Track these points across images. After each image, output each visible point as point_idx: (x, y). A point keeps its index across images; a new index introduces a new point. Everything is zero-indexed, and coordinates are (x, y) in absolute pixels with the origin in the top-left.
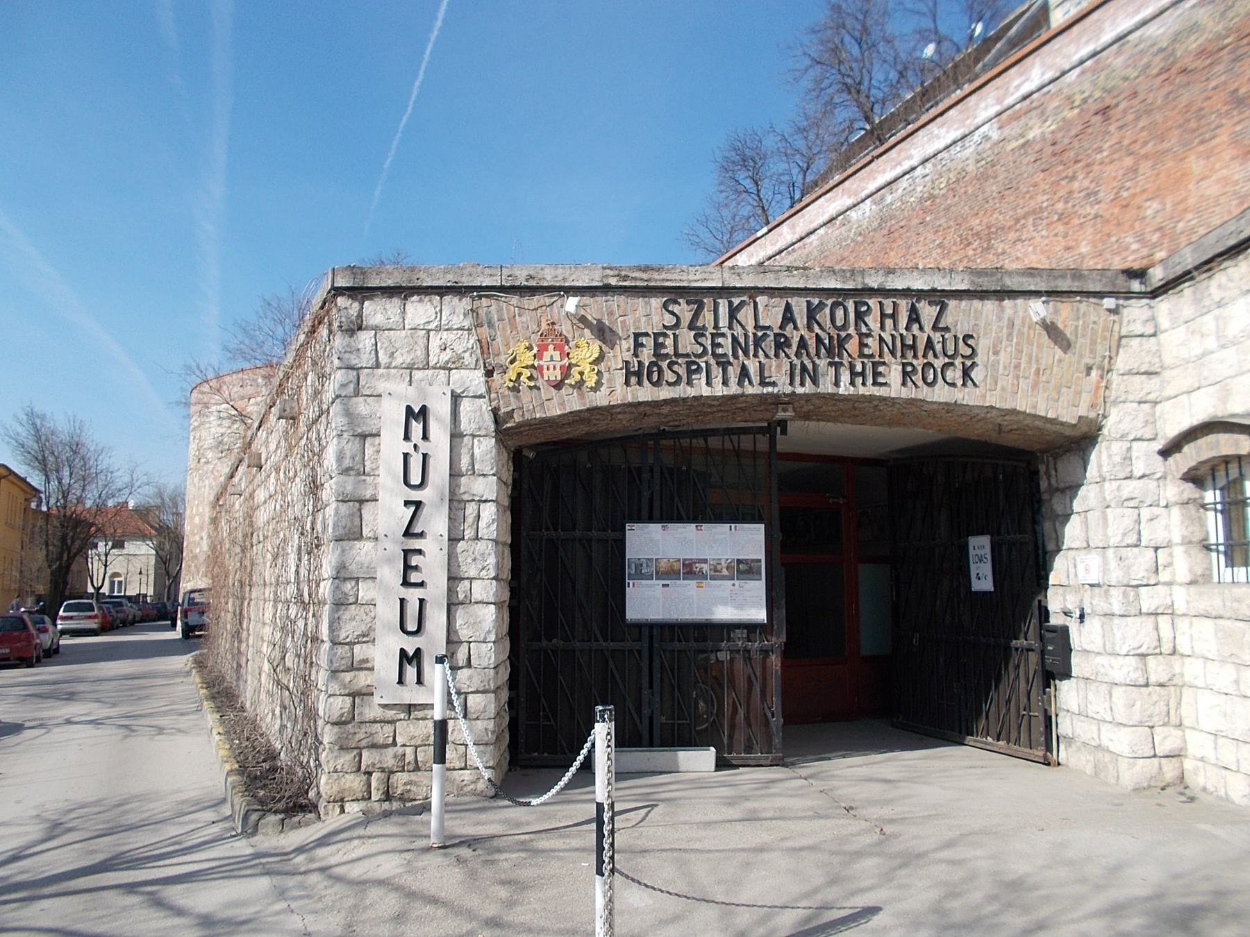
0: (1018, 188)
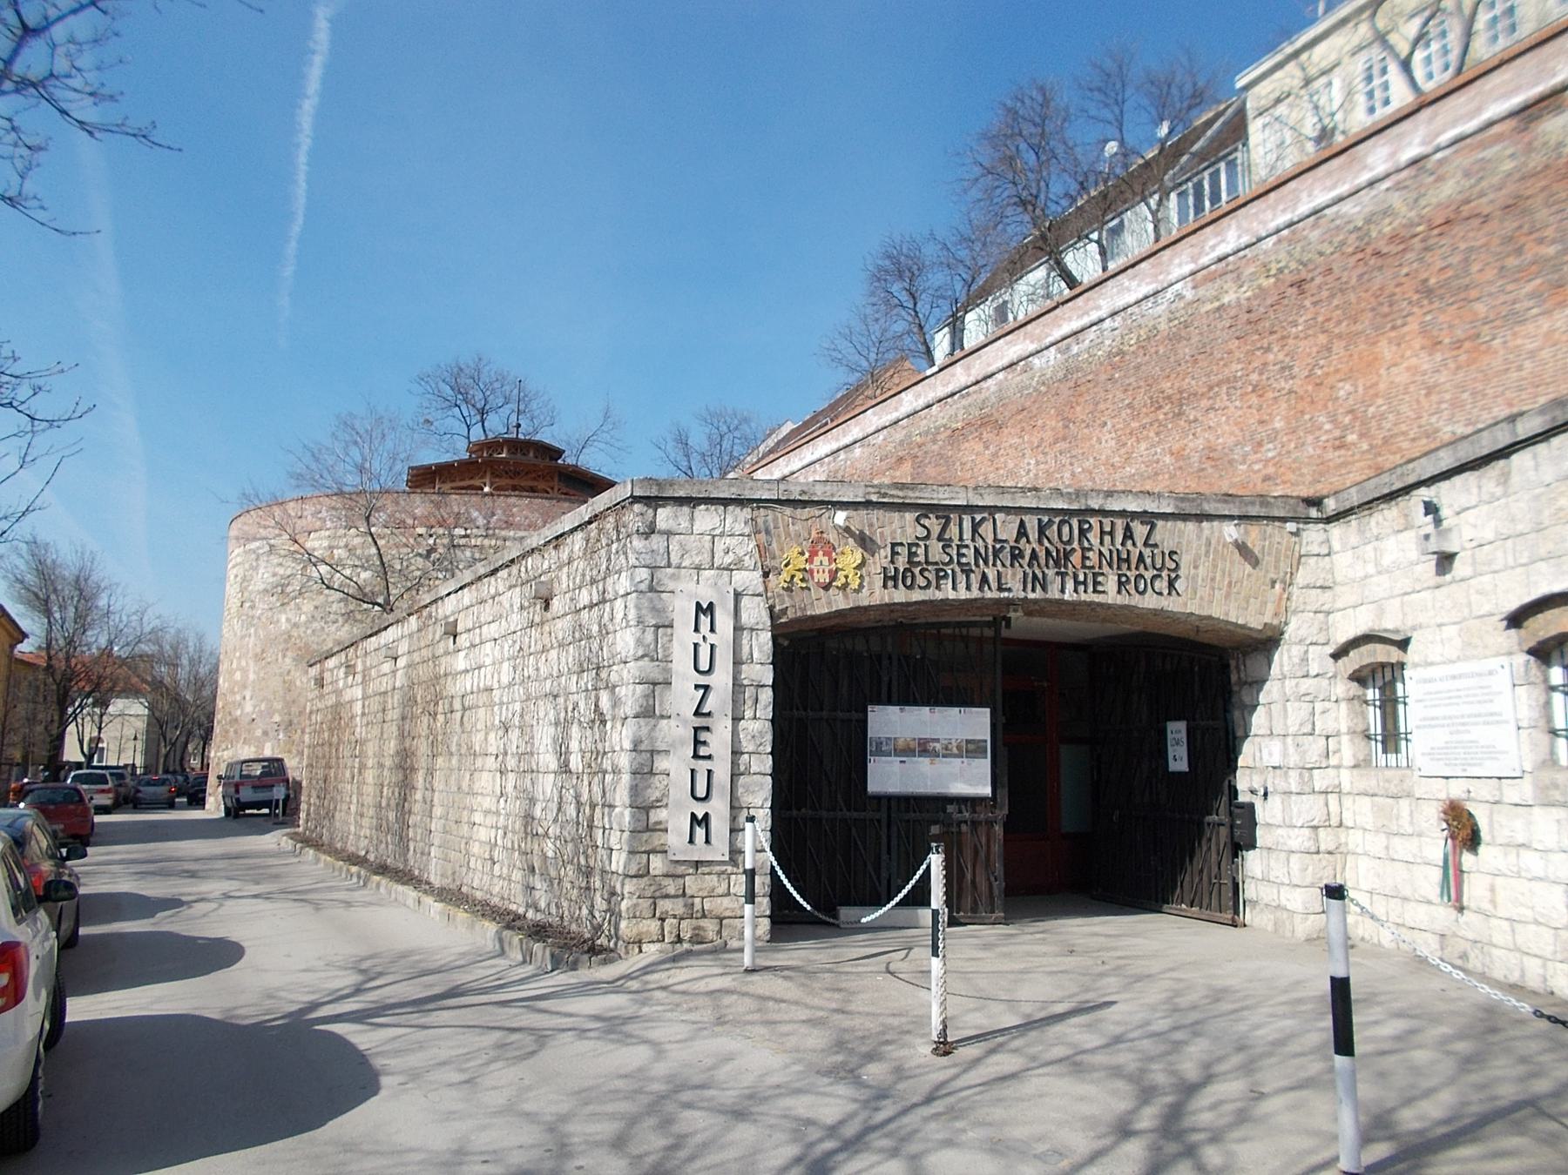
0: (1212, 354)
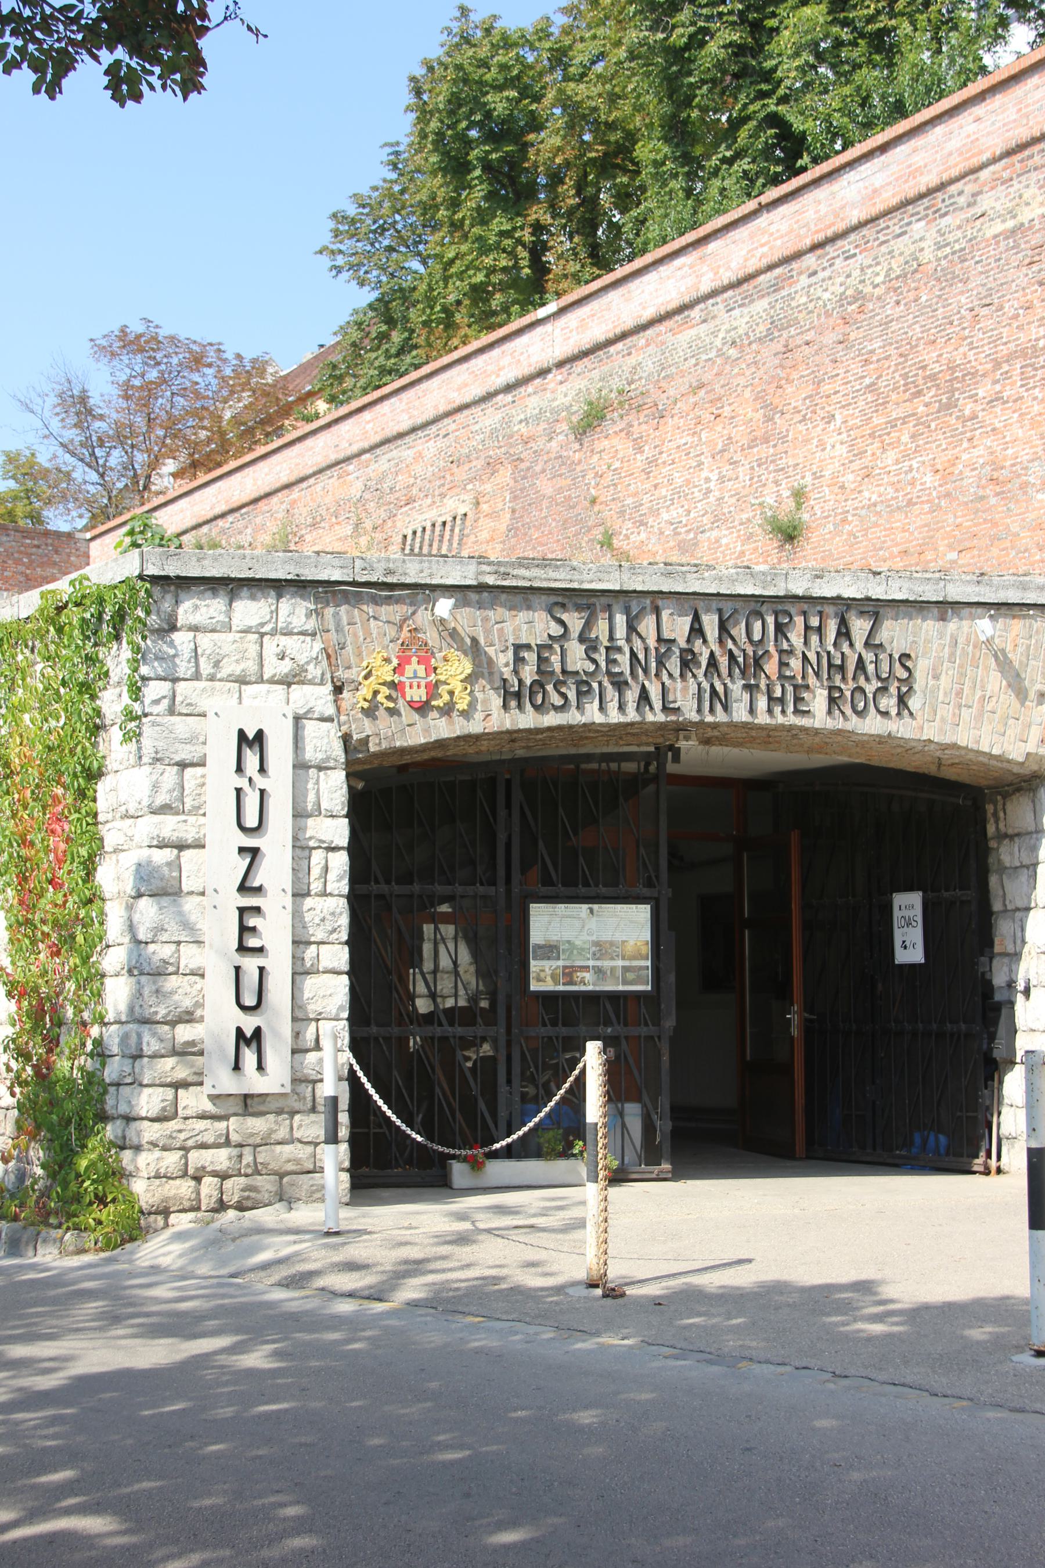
0: (1001, 308)
